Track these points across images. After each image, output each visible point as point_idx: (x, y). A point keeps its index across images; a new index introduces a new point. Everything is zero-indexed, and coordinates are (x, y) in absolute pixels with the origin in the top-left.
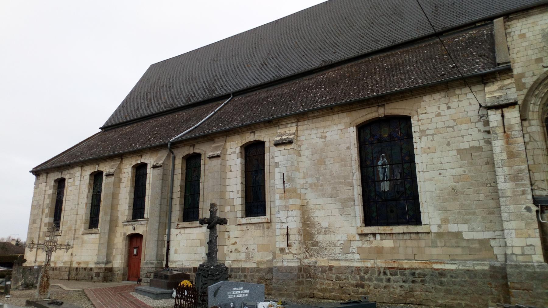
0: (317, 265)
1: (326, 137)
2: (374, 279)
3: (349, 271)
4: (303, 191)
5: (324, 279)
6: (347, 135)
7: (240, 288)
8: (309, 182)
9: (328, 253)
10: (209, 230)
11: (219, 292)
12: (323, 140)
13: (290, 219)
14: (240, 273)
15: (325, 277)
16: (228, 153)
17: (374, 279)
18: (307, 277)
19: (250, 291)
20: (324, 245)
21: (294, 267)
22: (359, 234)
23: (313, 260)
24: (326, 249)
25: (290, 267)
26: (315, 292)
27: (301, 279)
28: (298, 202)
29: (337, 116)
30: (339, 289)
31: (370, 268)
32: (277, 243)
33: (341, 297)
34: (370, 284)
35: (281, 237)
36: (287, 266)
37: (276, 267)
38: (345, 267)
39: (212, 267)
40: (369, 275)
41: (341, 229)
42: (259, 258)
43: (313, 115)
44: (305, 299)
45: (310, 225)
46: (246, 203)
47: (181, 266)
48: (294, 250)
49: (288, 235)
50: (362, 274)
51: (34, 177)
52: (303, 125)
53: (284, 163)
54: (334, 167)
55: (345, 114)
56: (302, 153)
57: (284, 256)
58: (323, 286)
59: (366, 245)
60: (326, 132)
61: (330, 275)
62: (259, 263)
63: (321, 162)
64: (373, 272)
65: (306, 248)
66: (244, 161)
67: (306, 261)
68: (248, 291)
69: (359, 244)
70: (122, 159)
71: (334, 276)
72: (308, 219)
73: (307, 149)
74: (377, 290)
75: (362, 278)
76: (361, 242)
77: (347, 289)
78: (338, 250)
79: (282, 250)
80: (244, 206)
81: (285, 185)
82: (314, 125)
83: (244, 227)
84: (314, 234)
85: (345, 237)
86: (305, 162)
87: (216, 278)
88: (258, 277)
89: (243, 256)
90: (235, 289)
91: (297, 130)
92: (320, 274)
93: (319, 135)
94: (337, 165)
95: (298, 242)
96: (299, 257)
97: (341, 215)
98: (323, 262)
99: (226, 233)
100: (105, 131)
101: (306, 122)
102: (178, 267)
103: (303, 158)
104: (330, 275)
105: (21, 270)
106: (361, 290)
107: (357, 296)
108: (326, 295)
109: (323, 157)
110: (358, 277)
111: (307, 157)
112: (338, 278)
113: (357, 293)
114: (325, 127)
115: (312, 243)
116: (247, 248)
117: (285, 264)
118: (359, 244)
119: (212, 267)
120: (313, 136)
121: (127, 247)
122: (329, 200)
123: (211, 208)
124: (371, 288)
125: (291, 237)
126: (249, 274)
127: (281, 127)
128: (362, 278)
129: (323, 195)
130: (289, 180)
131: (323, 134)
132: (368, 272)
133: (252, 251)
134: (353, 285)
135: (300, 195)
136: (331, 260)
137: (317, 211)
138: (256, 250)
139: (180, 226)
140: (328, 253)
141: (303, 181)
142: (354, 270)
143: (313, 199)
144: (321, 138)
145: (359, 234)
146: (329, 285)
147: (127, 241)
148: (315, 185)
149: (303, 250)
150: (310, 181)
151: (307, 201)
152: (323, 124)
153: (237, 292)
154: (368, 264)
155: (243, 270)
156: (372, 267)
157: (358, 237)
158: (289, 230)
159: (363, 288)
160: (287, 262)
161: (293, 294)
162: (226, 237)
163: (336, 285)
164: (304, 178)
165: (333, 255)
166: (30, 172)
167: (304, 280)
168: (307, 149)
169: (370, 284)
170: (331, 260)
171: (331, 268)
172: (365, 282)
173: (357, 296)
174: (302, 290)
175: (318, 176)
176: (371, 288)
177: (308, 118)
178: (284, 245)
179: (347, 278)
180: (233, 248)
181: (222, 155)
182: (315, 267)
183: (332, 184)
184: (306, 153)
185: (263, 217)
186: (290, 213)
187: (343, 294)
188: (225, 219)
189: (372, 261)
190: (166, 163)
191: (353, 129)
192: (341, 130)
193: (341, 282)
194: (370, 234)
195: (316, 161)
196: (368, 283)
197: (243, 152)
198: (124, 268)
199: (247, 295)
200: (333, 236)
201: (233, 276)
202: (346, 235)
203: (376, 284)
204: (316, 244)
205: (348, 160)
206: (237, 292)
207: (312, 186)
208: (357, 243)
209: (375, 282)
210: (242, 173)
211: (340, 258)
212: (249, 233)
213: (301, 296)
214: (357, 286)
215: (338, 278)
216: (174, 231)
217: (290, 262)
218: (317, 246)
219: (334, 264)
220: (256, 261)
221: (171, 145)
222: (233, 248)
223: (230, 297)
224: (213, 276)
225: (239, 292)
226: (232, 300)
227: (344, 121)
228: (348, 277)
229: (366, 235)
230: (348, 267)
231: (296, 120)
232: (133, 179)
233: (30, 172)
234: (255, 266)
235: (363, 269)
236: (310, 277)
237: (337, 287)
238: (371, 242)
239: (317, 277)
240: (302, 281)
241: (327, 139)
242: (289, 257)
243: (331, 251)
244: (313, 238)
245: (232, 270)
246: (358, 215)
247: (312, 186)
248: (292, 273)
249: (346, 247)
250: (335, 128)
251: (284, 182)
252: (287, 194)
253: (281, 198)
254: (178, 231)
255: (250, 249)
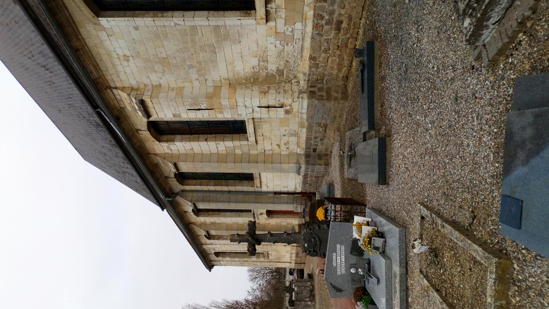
0: (308, 73)
1: (125, 55)
2: (331, 8)
3: (318, 38)
4: (210, 83)
5: (326, 66)
6: (116, 30)
7: (334, 258)
8: (197, 77)
9: (293, 59)
10: (263, 243)
11: (338, 286)
12: (131, 58)
13: (248, 104)
14: (312, 142)
15: (323, 65)
16: (170, 152)
17: (331, 8)
18: (322, 82)
19: (338, 243)
20: (282, 63)
21: (308, 103)
22: (267, 22)
23: (301, 76)
24: (287, 61)
25: (308, 106)
26: (341, 75)
27: (324, 94)
28: (225, 91)
29: (87, 41)
30: (341, 51)
31: (315, 13)
32: (279, 116)
33: (351, 49)
34: (337, 13)
35: (271, 113)
36: (308, 109)
37: (307, 120)
38: (312, 42)
39: (306, 245)
40: (325, 14)
41: (260, 43)
42: (297, 126)
43: (94, 72)
44: (350, 90)
45: (256, 77)
46: (230, 133)
47: (301, 184)
48: (288, 101)
49: (268, 107)
50: (323, 22)
51: (215, 267)
52: (114, 81)
53: (173, 109)
54: (170, 47)
55: (81, 30)
56: (155, 83)
57: (295, 110)
58: (335, 67)
59: (282, 13)
60: (118, 55)
61: (321, 59)
62: (301, 126)
63: (165, 62)
64: (322, 8)
65: (286, 83)
66: (178, 137)
67: (302, 83)
68: (338, 246)
69: (280, 23)
70: (190, 223)
71: (323, 55)
72: (247, 79)
73: (148, 77)
74: (347, 4)
75: (328, 23)
76: (277, 20)
77: (342, 41)
78: (289, 48)
79: (287, 112)
80: (235, 135)
81: (203, 108)
82: (110, 69)
83: (259, 138)
84: (268, 73)
85: (272, 40)
86: (168, 80)
87: (318, 242)
88: (318, 128)
89: (293, 139)
90: (334, 264)
91: (123, 89)
92: (319, 70)
93: (125, 63)
94: (165, 43)
95: (278, 95)
96: (296, 94)
97: (240, 42)
98: (305, 66)
99: (266, 152)
100: (165, 206)
101: (108, 78)
102: (301, 186)
103: (163, 82)
104: (321, 59)
105: (298, 303)
106: (344, 25)
107: (352, 30)
108: (346, 65)
109: (157, 60)
110: (326, 28)
111: (161, 78)
112: (326, 51)
113: (348, 30)
114: (110, 56)
115: (279, 76)
116: (284, 136)
117: (304, 111)
118: (280, 23)
119: (306, 245)
120: (128, 70)
121: (279, 216)
122: (220, 56)
123: (235, 241)
124: (343, 12)
125: (271, 103)
126: (313, 134)
127: (123, 106)
128: (328, 23)
129: (214, 62)
130: (195, 104)
131: (122, 58)
132: (321, 15)
133: (287, 132)
134: (337, 34)
135: (215, 87)
136: (302, 57)
137: (236, 69)
138: (286, 128)
139: (259, 186)
140: (293, 59)
141: (196, 84)
142: (316, 32)
143: (220, 72)
144: (128, 61)
145: (267, 22)
146: (333, 62)
147: (274, 216)
148: (200, 70)
149: (287, 86)
150: (194, 76)
151: (223, 80)
152: (105, 58)
153: (339, 261)
154: (310, 13)
155: (308, 139)
156: (314, 10)
157: (271, 24)
158: (263, 105)
159: (342, 22)
160: (302, 109)
161: (341, 105)
162: (271, 152)
163: (335, 53)
164: (191, 82)
165: (296, 54)
166: (210, 271)
167: (325, 87)
168: (148, 77)
169: (337, 13)
170: (302, 57)
171: (312, 58)
172: (335, 20)
173: (352, 30)
174: (337, 92)
175: (186, 67)
176: (343, 12)
177: (102, 76)
178: (281, 110)
179: (327, 41)
180: (283, 147)
181: (174, 160)
182: (309, 75)
183: (195, 51)
184: (154, 79)
185: (247, 123)
186: (240, 104)
187: (347, 46)
188: (249, 225)
189: (306, 9)
190: (190, 198)
191: (103, 21)
192: (108, 36)
193: (331, 48)
194: (266, 7)
195: (164, 68)
196: (336, 15)
197: (165, 137)
198: (300, 218)
199: (343, 248)
200: (269, 53)
201: (315, 147)
202: (268, 38)
203: (338, 6)
204: (280, 72)
205: (155, 29)
206: (339, 261)
207: (202, 72)
208: (280, 24)
209: (336, 7)
210: (194, 140)
211: (300, 46)
212: (267, 134)
213: (345, 96)
214: (338, 29)
215: (326, 51)
216: (264, 189)
217: (302, 106)
218: (283, 71)
219: (307, 54)
220: (300, 129)
221: (169, 197)
222: (283, 147)
223: (343, 272)
224: (316, 245)
225: (339, 258)
226: (348, 269)
227: (93, 32)
228: (325, 40)
229: (267, 13)
230: (312, 38)
231: (109, 90)
232: (211, 215)
233: (210, 271)
234: (304, 130)
235: (316, 21)
236: (322, 80)
237: (338, 52)
238: (278, 7)
239: (323, 73)
240: (327, 92)
241: (128, 54)
242: (295, 107)
243: (290, 56)
244: (272, 75)
245: (307, 148)
246: (239, 22)
247: (202, 72)
248: (315, 106)
249: (285, 39)
250: (107, 43)
251: (199, 110)
252: (215, 107)
253: (222, 113)
254: (263, 184)
255: (283, 132)
